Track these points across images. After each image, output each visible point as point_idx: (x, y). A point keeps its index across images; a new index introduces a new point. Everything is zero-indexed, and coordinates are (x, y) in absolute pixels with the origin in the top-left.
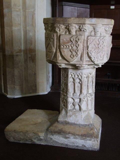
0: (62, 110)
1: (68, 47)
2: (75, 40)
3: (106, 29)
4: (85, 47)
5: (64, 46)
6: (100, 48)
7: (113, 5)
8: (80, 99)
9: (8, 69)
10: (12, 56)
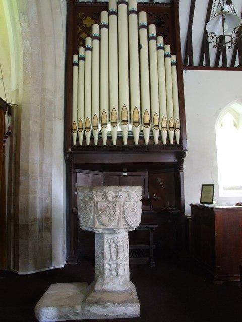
0: (98, 278)
7: (125, 172)
8: (117, 264)
9: (21, 242)
10: (26, 226)
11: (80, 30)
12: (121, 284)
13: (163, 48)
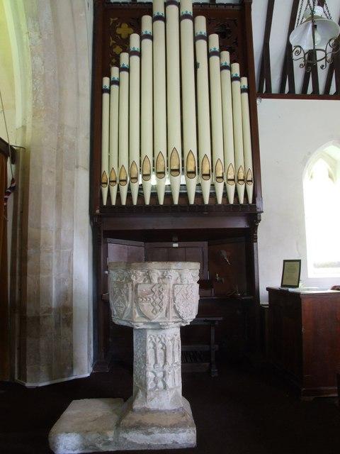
0: (137, 391)
7: (176, 242)
8: (164, 373)
9: (29, 341)
10: (37, 319)
11: (112, 42)
13: (230, 68)
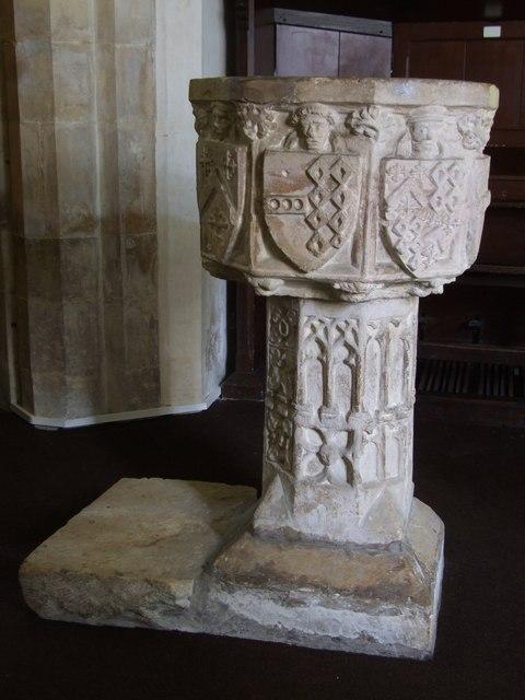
0: (271, 480)
1: (296, 204)
2: (326, 175)
3: (464, 129)
4: (370, 206)
5: (281, 200)
6: (436, 209)
7: (493, 22)
8: (351, 434)
9: (33, 303)
10: (52, 247)
12: (362, 517)
